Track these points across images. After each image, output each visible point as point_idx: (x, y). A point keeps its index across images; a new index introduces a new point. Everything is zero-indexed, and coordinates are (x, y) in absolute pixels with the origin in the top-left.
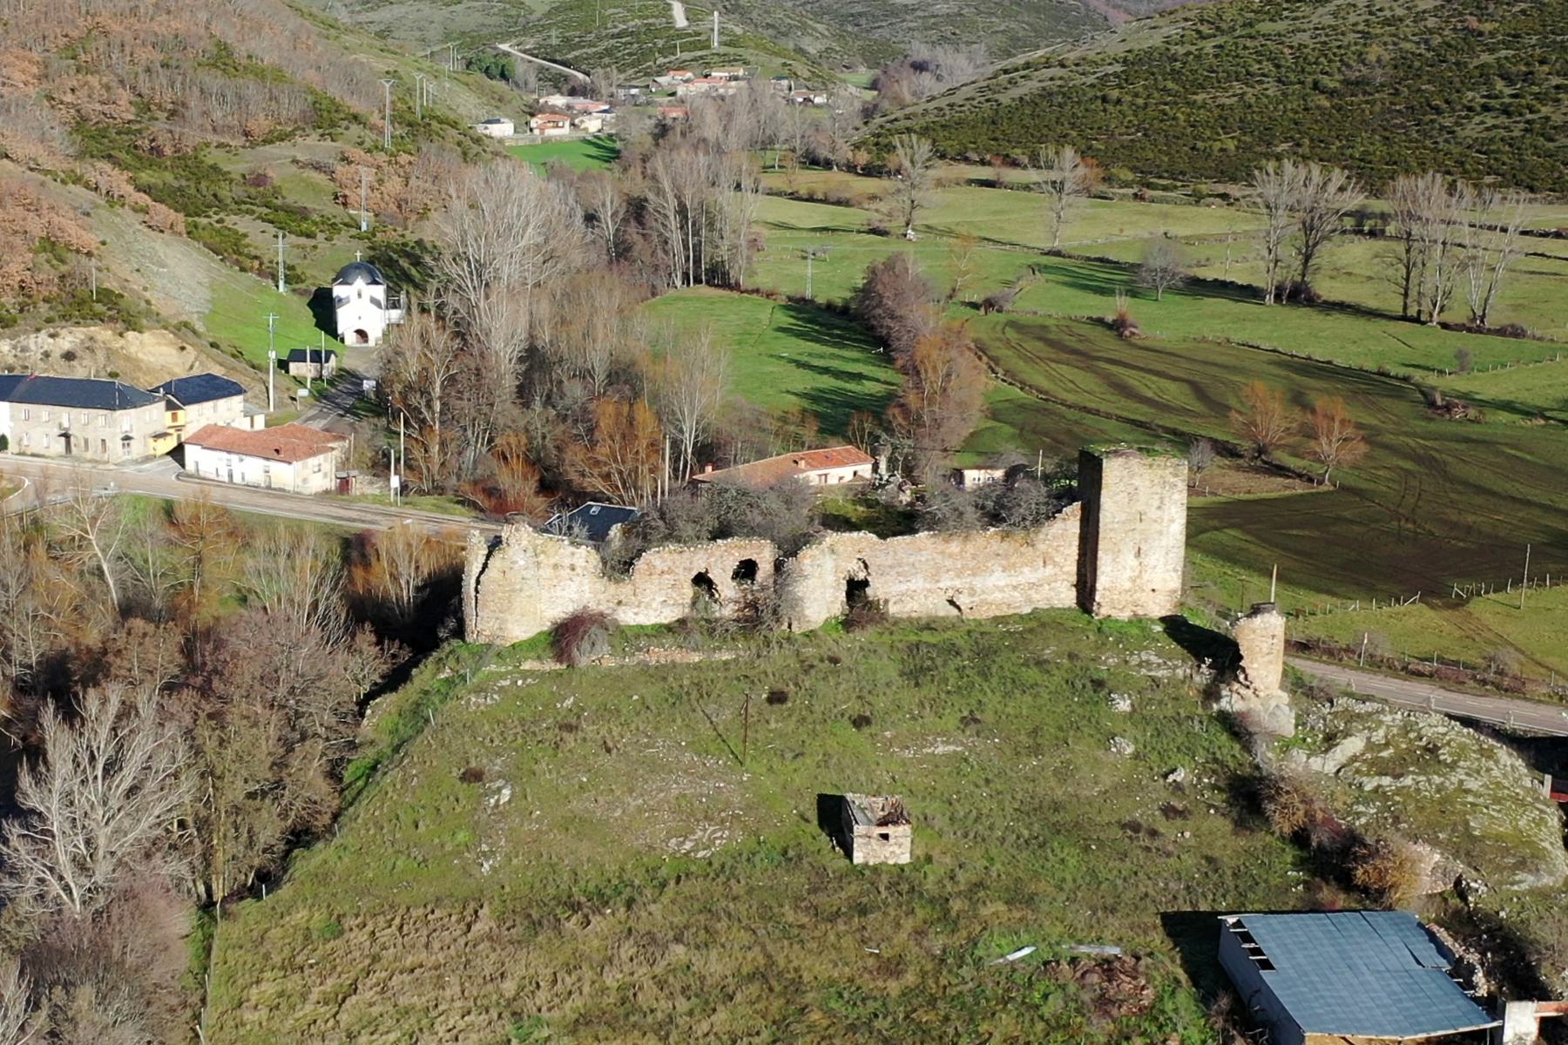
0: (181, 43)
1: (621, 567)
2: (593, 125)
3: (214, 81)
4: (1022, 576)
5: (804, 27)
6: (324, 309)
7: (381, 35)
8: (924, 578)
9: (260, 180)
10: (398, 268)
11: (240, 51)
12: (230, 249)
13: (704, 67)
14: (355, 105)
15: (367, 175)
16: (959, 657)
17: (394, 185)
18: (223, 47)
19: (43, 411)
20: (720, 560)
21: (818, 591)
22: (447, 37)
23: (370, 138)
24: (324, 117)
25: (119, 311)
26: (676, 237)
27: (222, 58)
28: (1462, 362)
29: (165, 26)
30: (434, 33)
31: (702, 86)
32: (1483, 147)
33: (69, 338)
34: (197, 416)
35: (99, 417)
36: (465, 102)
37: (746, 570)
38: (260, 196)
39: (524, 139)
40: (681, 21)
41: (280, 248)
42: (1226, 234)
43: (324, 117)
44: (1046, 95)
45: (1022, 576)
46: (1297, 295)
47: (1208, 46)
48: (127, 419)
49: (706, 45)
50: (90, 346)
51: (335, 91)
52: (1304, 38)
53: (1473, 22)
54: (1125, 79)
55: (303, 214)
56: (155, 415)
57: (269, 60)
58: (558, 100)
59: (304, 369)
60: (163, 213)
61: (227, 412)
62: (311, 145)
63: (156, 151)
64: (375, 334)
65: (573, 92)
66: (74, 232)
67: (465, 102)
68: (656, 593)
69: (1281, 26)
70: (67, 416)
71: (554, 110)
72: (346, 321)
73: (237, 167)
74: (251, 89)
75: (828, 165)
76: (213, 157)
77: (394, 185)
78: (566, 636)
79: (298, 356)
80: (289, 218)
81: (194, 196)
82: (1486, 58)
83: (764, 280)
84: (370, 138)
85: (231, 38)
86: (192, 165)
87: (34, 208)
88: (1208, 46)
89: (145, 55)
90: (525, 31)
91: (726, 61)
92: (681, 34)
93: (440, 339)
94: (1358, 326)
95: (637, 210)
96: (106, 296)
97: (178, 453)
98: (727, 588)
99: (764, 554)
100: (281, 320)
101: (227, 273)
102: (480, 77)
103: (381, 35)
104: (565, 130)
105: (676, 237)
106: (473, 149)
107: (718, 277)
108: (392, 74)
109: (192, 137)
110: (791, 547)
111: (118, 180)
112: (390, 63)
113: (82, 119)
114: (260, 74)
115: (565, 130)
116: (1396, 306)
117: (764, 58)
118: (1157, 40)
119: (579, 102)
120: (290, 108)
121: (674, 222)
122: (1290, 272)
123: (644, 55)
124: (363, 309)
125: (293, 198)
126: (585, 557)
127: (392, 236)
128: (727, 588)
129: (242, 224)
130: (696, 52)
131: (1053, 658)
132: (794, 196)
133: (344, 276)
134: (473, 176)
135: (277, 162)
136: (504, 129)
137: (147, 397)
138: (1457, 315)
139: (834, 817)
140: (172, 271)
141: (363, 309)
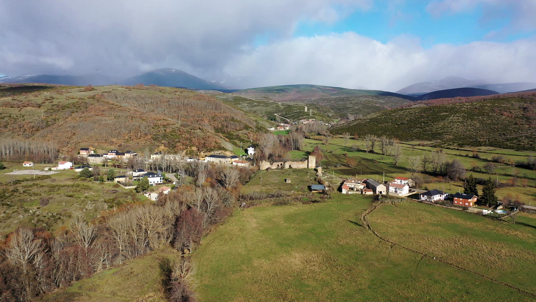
0: (227, 117)
1: (272, 164)
2: (287, 128)
3: (232, 122)
4: (302, 165)
5: (329, 111)
6: (246, 151)
7: (254, 112)
8: (296, 165)
9: (238, 135)
10: (254, 146)
11: (235, 118)
12: (235, 144)
13: (308, 119)
14: (250, 126)
15: (252, 135)
16: (296, 171)
17: (255, 136)
18: (233, 118)
19: (218, 159)
20: (279, 163)
21: (287, 166)
22: (266, 112)
23: (252, 130)
24: (246, 127)
25: (226, 150)
26: (292, 144)
27: (233, 119)
28: (382, 159)
29: (224, 115)
30: (264, 112)
31: (307, 122)
32: (416, 133)
33: (219, 152)
34: (234, 160)
35: (224, 159)
36: (267, 125)
37: (281, 164)
38: (238, 137)
39: (276, 130)
40: (306, 110)
41: (241, 144)
42: (363, 144)
43: (246, 127)
44: (357, 124)
45: (302, 165)
46: (371, 152)
47: (383, 117)
48: (227, 159)
49: (309, 115)
50: (222, 153)
51: (248, 124)
52: (397, 116)
53: (423, 114)
54: (369, 122)
55: (244, 140)
56: (229, 159)
57: (239, 119)
58: (282, 124)
59: (244, 157)
60: (227, 139)
61: (237, 159)
62: (245, 131)
63: (224, 132)
64: (253, 154)
65: (285, 123)
66: (218, 141)
67: (267, 125)
68: (274, 166)
69: (395, 114)
70: (220, 159)
71: (281, 126)
72: (249, 152)
73: (235, 134)
74: (237, 124)
75: (321, 135)
76: (232, 132)
77: (255, 136)
78: (267, 169)
79: (244, 156)
80: (242, 140)
81: (230, 137)
82: (423, 120)
83: (304, 150)
84: (252, 130)
85: (233, 116)
86: (229, 133)
87: (213, 138)
88: (383, 117)
89: (223, 119)
90: (279, 112)
91: (312, 118)
92: (306, 113)
93: (260, 152)
94: (377, 155)
95: (288, 140)
96: (223, 147)
97: (232, 163)
98: (280, 166)
99: (283, 163)
100: (241, 152)
101: (235, 147)
102: (270, 121)
103: (254, 112)
104: (283, 129)
105: (292, 144)
106: (267, 131)
107: (298, 149)
108: (256, 121)
109: (229, 130)
110: (284, 163)
111: (221, 135)
112: (255, 119)
113: (215, 127)
114: (238, 122)
115: (283, 129)
116: (381, 152)
117: (318, 117)
118: (376, 116)
119: (286, 125)
120: (242, 126)
121: (292, 142)
122: (371, 149)
123: (299, 116)
124: (251, 151)
125: (242, 138)
126: (269, 163)
127: (255, 143)
128: (280, 166)
129: (236, 141)
130: (307, 116)
131: (306, 171)
132: (314, 139)
133: (249, 147)
134: (265, 135)
135: (240, 133)
136: (273, 129)
137: (229, 157)
138: (388, 154)
139: (285, 180)
140: (228, 145)
141: (251, 151)
